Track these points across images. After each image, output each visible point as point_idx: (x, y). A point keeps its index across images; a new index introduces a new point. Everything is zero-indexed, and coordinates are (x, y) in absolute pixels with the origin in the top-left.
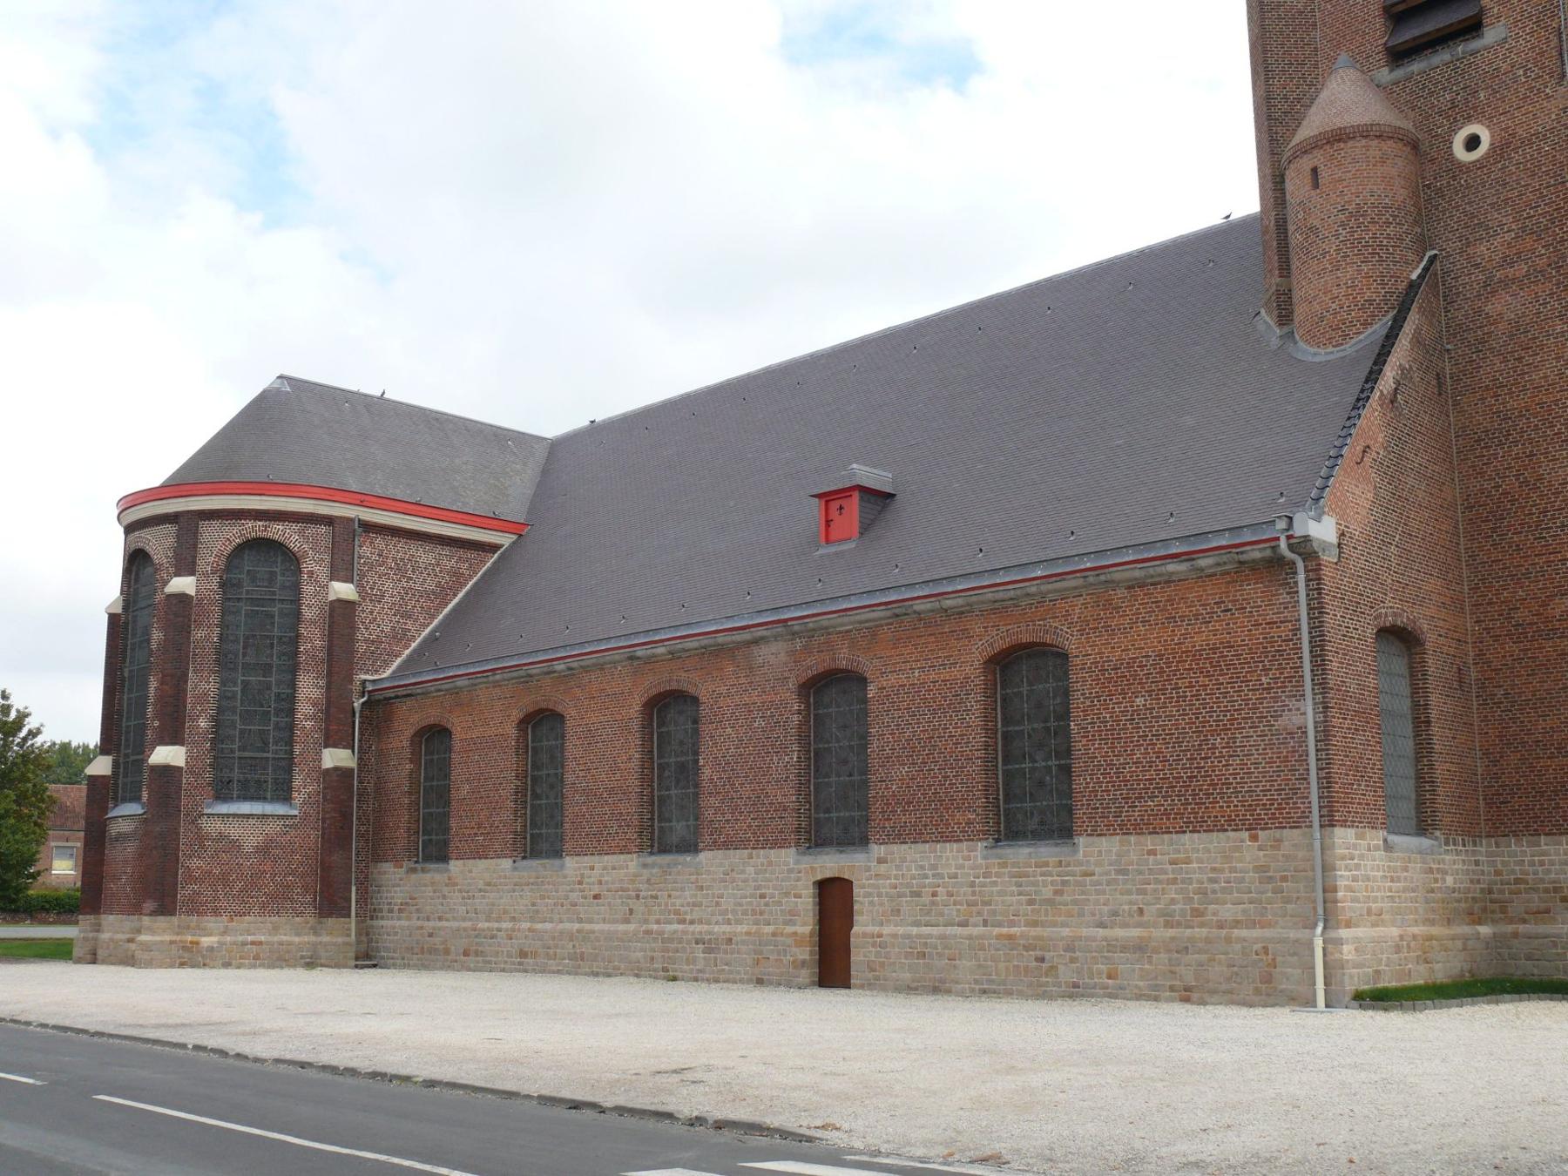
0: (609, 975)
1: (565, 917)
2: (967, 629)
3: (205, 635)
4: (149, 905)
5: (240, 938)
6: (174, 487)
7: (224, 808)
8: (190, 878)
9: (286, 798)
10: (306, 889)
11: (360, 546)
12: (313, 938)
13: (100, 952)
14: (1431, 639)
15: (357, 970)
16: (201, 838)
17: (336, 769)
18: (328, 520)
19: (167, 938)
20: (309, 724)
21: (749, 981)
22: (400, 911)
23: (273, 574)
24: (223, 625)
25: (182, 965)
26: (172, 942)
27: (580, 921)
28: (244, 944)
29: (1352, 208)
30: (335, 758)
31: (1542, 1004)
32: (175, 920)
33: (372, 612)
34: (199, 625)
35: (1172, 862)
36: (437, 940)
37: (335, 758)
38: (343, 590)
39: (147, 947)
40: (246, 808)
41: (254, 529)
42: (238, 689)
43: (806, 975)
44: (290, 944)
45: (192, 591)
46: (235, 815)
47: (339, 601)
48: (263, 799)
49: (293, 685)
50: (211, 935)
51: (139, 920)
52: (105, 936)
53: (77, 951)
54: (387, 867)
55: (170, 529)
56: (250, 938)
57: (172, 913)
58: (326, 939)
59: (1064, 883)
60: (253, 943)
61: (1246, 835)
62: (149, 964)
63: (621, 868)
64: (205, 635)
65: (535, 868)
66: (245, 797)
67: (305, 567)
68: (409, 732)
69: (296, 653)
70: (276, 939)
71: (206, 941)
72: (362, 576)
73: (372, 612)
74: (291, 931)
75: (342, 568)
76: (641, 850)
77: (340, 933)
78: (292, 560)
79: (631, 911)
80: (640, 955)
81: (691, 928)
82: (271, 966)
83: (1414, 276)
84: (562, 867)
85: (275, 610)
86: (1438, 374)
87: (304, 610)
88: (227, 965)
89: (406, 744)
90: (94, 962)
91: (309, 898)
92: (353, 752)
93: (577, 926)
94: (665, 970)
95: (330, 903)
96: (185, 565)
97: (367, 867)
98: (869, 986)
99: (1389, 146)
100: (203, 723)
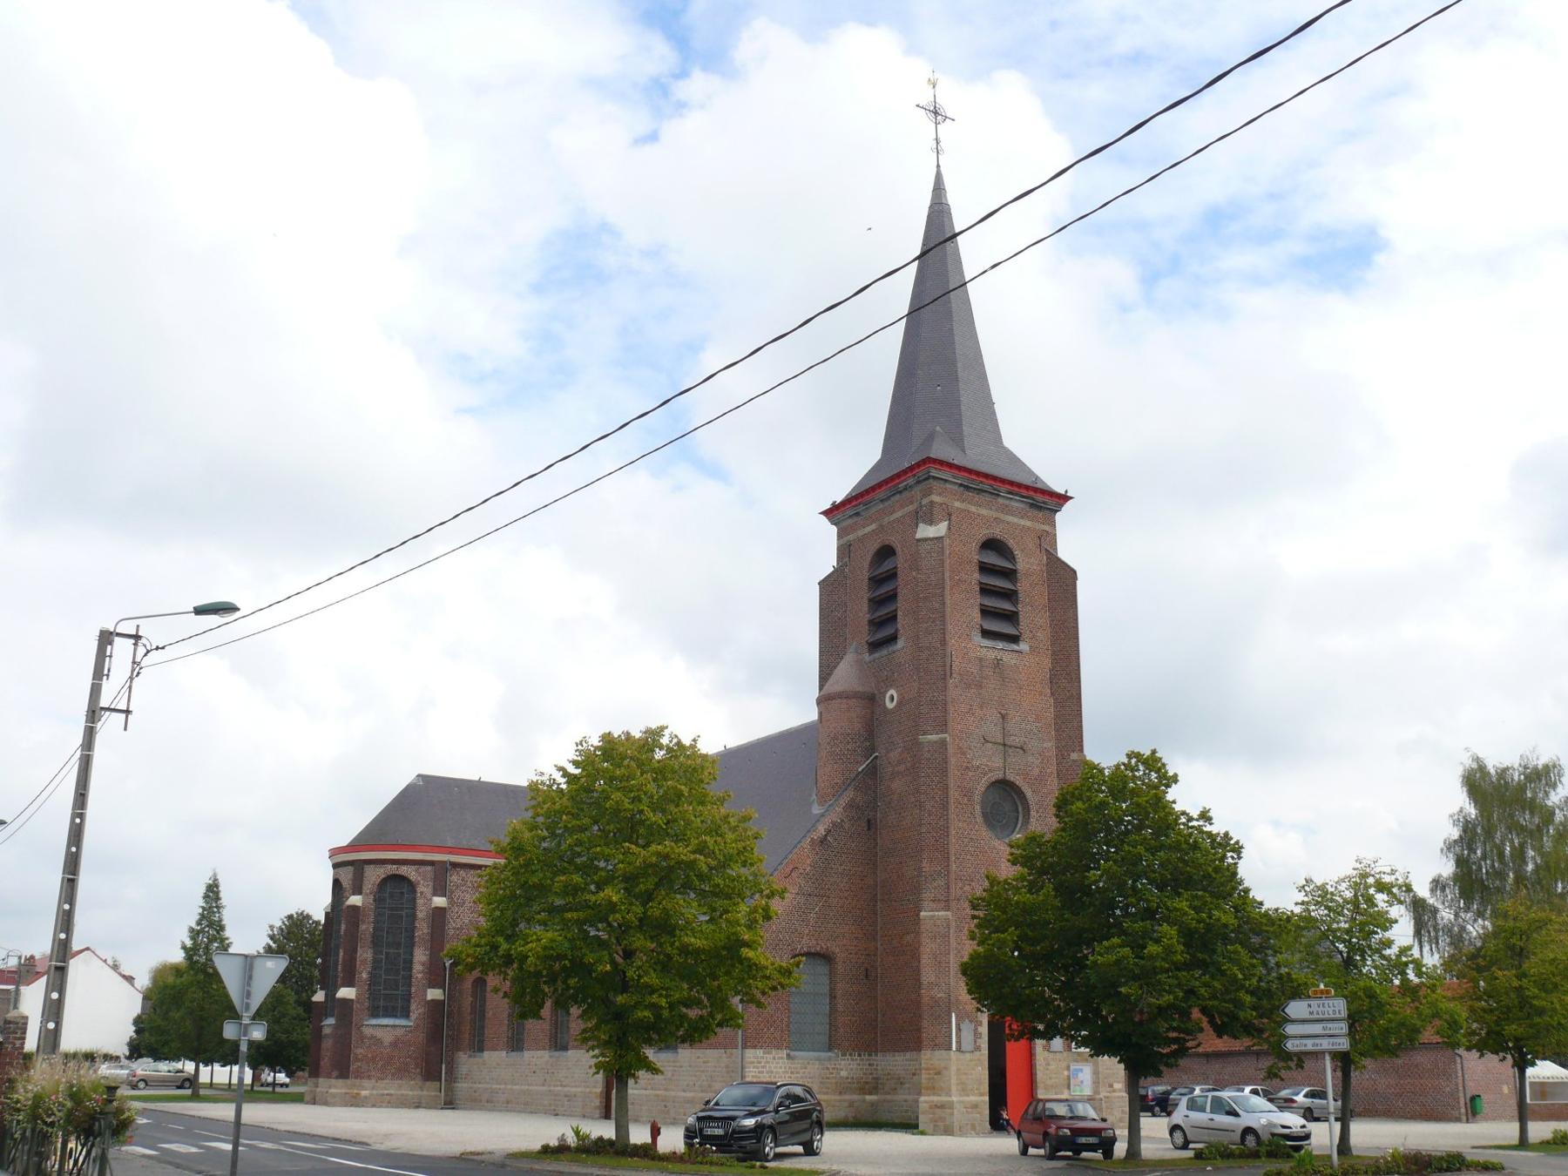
3: (367, 928)
4: (335, 1073)
5: (381, 1092)
6: (353, 847)
7: (374, 1022)
8: (357, 1060)
9: (407, 1016)
10: (417, 1066)
11: (451, 876)
12: (420, 1093)
13: (317, 1099)
14: (840, 956)
16: (362, 1038)
17: (432, 1000)
18: (432, 863)
19: (344, 1091)
20: (420, 976)
21: (580, 1116)
22: (465, 1078)
23: (402, 893)
24: (376, 922)
25: (351, 1106)
26: (346, 1093)
28: (383, 1095)
29: (832, 735)
30: (434, 994)
31: (853, 1132)
32: (348, 1082)
33: (457, 913)
34: (364, 922)
35: (704, 1062)
36: (477, 1094)
37: (434, 994)
38: (440, 901)
39: (334, 1096)
40: (385, 1021)
41: (392, 869)
42: (383, 957)
43: (597, 1113)
44: (407, 1095)
45: (359, 904)
46: (379, 1025)
47: (436, 908)
48: (395, 1016)
49: (412, 955)
50: (366, 1090)
52: (318, 1090)
53: (307, 1098)
54: (461, 1054)
55: (351, 868)
56: (386, 1092)
57: (347, 1077)
58: (425, 1093)
59: (675, 1071)
60: (387, 1095)
61: (723, 1051)
62: (334, 1105)
63: (541, 1058)
64: (367, 928)
66: (385, 1016)
67: (419, 890)
68: (471, 980)
69: (413, 937)
70: (399, 1092)
71: (364, 1093)
72: (452, 892)
73: (457, 913)
74: (408, 1088)
75: (440, 890)
76: (550, 1049)
77: (430, 1091)
78: (412, 886)
82: (397, 1107)
83: (860, 770)
85: (404, 913)
86: (869, 821)
87: (418, 913)
88: (373, 1106)
89: (470, 986)
90: (314, 1104)
91: (418, 1070)
92: (444, 991)
93: (527, 1087)
95: (430, 1073)
96: (357, 890)
97: (453, 1053)
99: (852, 702)
100: (365, 975)
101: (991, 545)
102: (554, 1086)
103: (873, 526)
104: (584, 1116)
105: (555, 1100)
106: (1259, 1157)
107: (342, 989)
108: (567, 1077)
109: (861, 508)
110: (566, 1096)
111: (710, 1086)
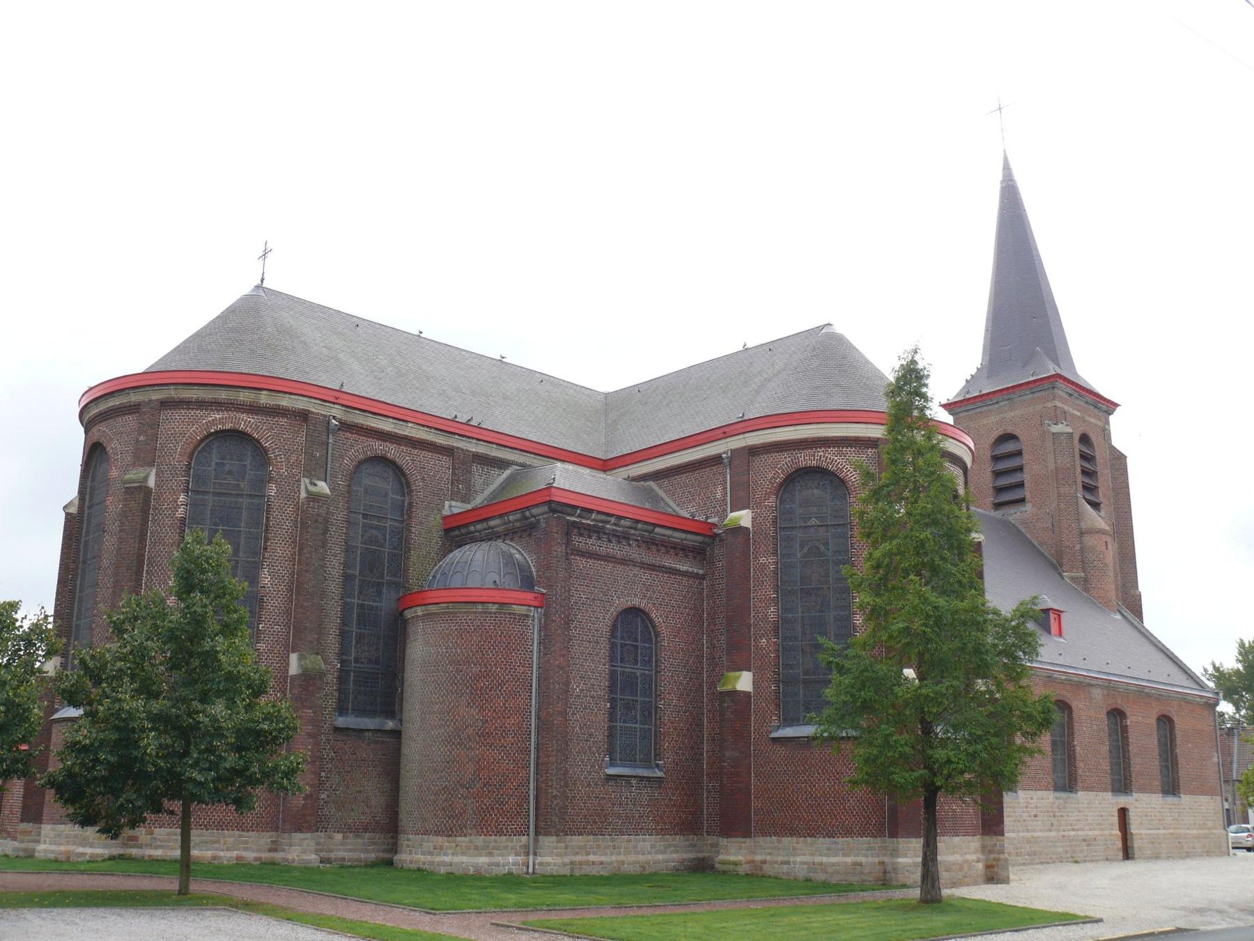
0: (1048, 863)
1: (1021, 828)
2: (456, 613)
15: (1107, 863)
27: (1028, 831)
51: (779, 842)
65: (1171, 799)
78: (261, 454)
79: (1052, 824)
80: (1061, 849)
81: (1079, 833)
84: (1017, 797)
94: (1072, 857)
98: (1140, 858)
101: (1008, 437)
102: (1064, 831)
103: (1078, 414)
104: (1107, 859)
105: (1071, 846)
106: (610, 721)
107: (912, 670)
108: (1078, 820)
109: (1012, 396)
110: (1084, 840)
111: (1205, 824)
